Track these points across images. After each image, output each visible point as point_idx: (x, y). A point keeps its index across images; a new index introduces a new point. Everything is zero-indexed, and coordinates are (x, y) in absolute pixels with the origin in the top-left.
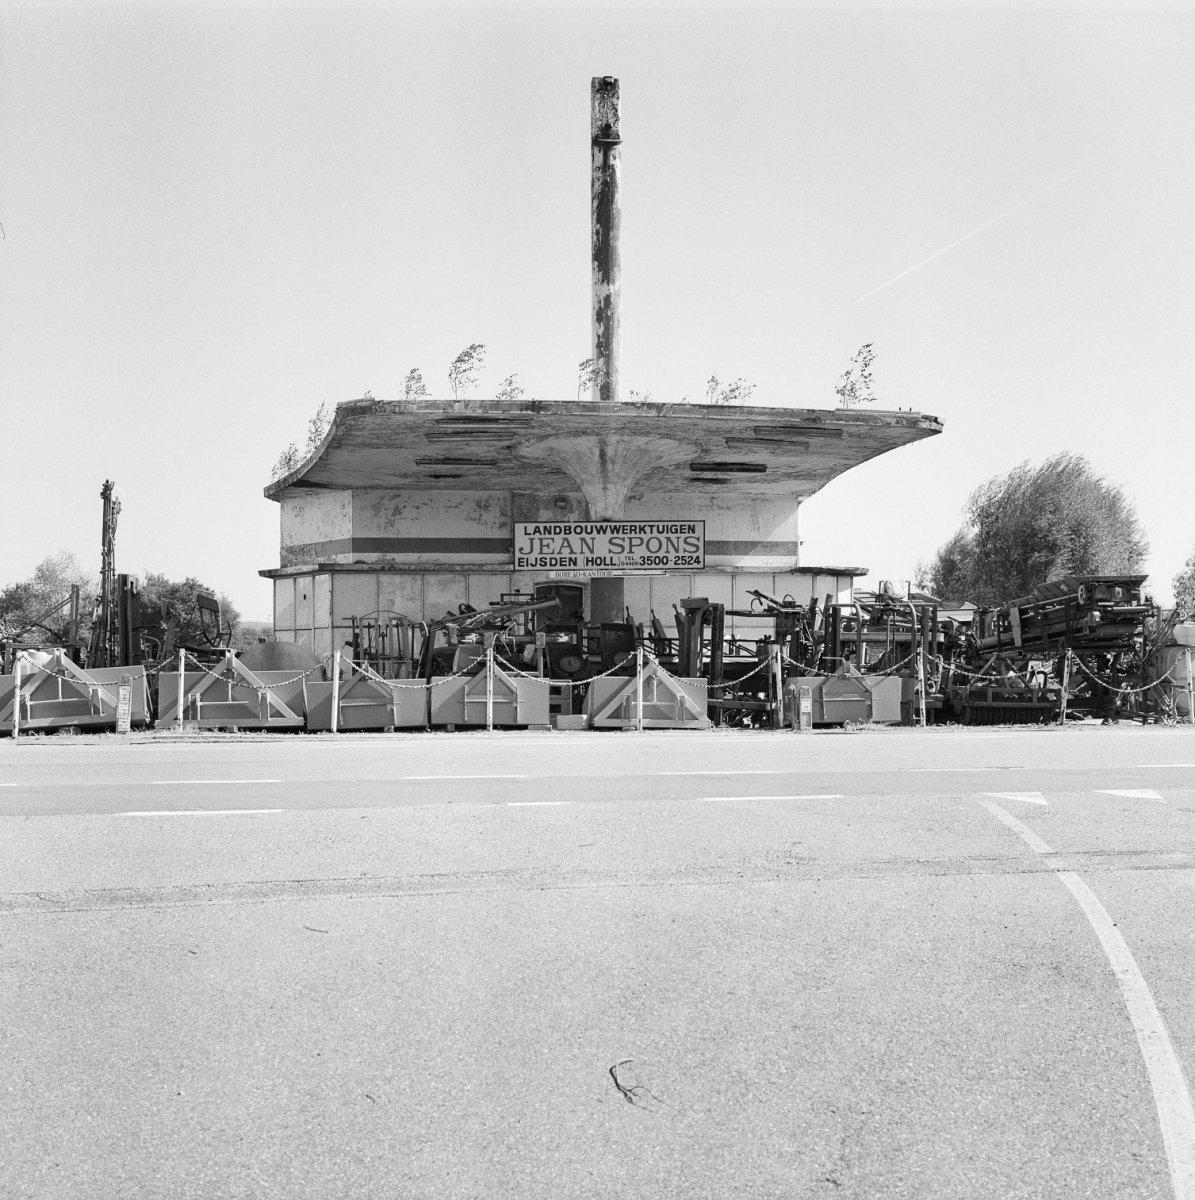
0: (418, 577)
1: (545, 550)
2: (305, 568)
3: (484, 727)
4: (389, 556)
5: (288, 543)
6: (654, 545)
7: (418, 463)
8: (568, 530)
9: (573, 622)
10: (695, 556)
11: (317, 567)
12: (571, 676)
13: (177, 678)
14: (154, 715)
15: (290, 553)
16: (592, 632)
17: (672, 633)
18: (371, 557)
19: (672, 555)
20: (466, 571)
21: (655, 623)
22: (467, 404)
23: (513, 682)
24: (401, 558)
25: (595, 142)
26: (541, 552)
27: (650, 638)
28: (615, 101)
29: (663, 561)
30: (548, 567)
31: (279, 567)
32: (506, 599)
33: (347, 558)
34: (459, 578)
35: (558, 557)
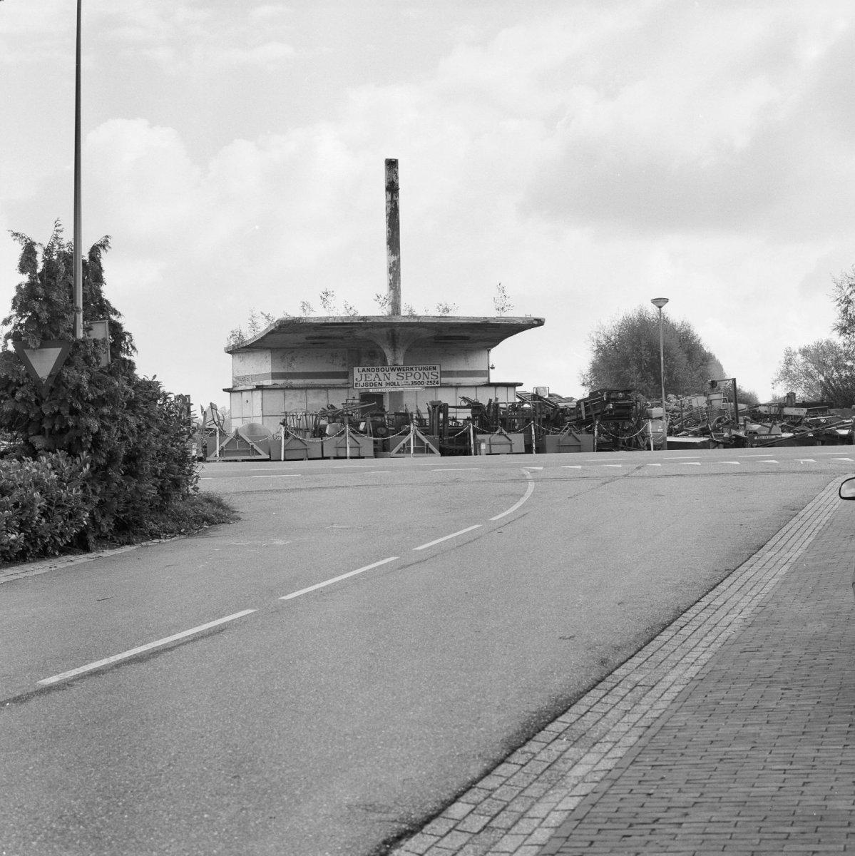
0: (304, 391)
1: (367, 379)
2: (248, 388)
3: (346, 458)
4: (289, 381)
5: (237, 375)
6: (417, 376)
7: (306, 338)
8: (378, 370)
9: (380, 412)
10: (436, 380)
11: (255, 387)
12: (382, 436)
13: (216, 439)
14: (205, 452)
15: (238, 379)
16: (390, 417)
17: (426, 416)
18: (281, 382)
19: (426, 380)
20: (327, 388)
21: (418, 412)
22: (335, 318)
23: (358, 439)
24: (296, 382)
25: (388, 189)
26: (366, 380)
27: (416, 419)
28: (396, 170)
29: (422, 383)
30: (369, 387)
31: (231, 387)
32: (349, 401)
33: (268, 382)
34: (323, 391)
35: (374, 382)
